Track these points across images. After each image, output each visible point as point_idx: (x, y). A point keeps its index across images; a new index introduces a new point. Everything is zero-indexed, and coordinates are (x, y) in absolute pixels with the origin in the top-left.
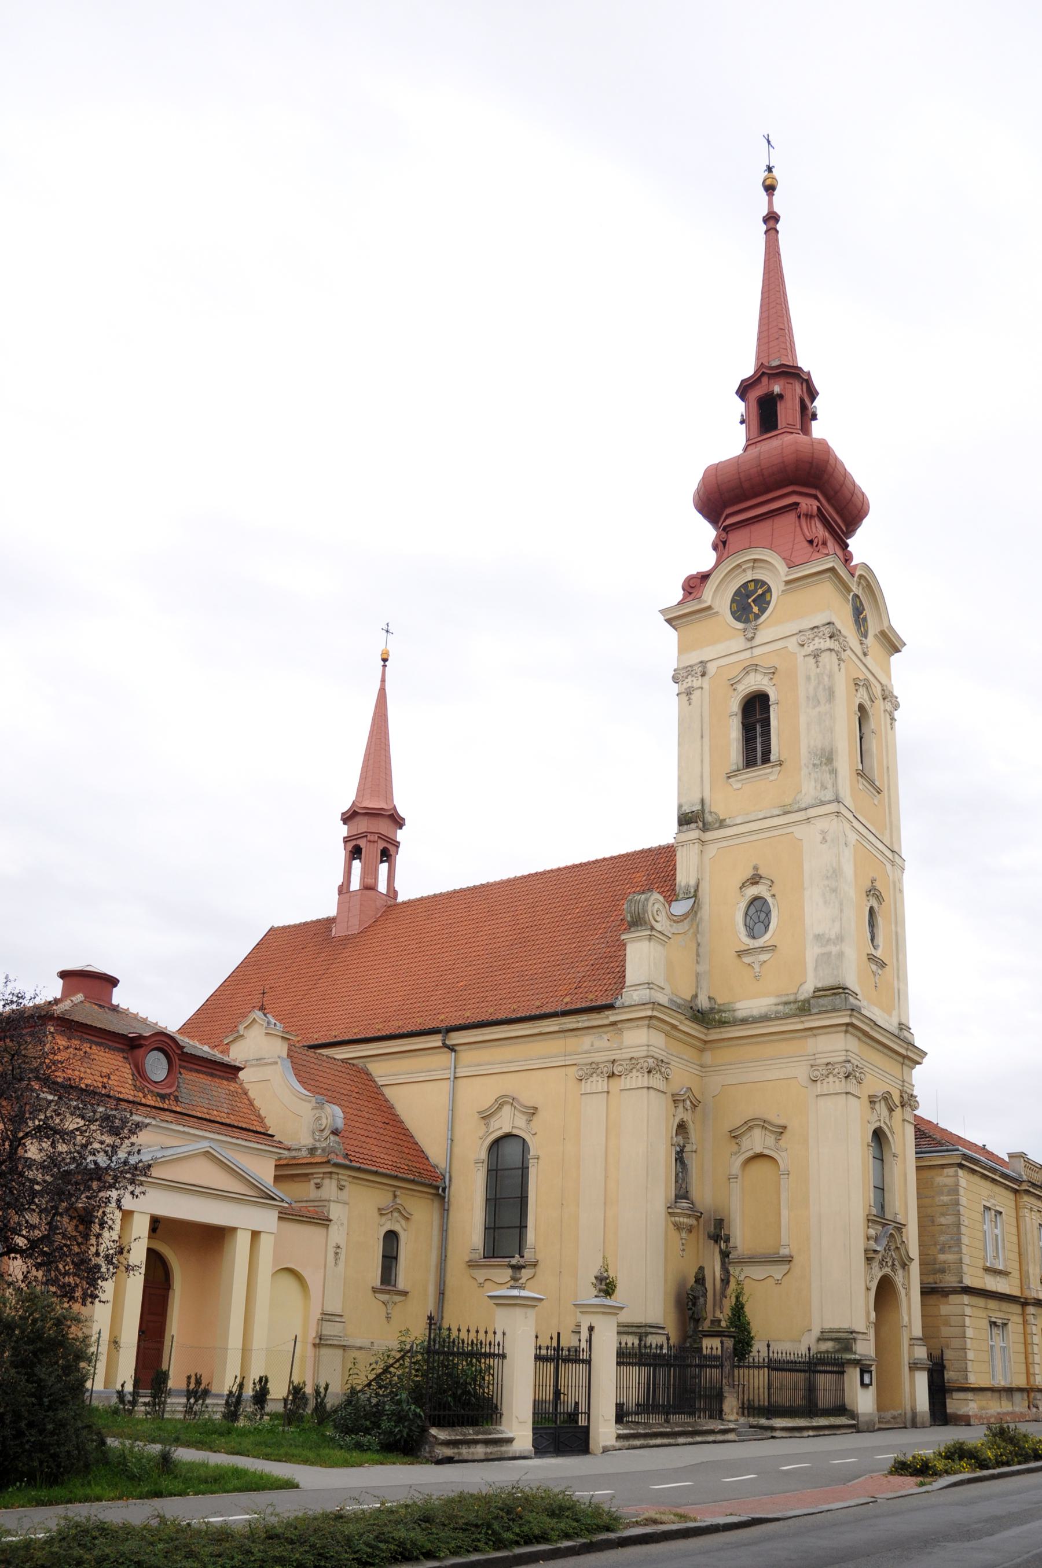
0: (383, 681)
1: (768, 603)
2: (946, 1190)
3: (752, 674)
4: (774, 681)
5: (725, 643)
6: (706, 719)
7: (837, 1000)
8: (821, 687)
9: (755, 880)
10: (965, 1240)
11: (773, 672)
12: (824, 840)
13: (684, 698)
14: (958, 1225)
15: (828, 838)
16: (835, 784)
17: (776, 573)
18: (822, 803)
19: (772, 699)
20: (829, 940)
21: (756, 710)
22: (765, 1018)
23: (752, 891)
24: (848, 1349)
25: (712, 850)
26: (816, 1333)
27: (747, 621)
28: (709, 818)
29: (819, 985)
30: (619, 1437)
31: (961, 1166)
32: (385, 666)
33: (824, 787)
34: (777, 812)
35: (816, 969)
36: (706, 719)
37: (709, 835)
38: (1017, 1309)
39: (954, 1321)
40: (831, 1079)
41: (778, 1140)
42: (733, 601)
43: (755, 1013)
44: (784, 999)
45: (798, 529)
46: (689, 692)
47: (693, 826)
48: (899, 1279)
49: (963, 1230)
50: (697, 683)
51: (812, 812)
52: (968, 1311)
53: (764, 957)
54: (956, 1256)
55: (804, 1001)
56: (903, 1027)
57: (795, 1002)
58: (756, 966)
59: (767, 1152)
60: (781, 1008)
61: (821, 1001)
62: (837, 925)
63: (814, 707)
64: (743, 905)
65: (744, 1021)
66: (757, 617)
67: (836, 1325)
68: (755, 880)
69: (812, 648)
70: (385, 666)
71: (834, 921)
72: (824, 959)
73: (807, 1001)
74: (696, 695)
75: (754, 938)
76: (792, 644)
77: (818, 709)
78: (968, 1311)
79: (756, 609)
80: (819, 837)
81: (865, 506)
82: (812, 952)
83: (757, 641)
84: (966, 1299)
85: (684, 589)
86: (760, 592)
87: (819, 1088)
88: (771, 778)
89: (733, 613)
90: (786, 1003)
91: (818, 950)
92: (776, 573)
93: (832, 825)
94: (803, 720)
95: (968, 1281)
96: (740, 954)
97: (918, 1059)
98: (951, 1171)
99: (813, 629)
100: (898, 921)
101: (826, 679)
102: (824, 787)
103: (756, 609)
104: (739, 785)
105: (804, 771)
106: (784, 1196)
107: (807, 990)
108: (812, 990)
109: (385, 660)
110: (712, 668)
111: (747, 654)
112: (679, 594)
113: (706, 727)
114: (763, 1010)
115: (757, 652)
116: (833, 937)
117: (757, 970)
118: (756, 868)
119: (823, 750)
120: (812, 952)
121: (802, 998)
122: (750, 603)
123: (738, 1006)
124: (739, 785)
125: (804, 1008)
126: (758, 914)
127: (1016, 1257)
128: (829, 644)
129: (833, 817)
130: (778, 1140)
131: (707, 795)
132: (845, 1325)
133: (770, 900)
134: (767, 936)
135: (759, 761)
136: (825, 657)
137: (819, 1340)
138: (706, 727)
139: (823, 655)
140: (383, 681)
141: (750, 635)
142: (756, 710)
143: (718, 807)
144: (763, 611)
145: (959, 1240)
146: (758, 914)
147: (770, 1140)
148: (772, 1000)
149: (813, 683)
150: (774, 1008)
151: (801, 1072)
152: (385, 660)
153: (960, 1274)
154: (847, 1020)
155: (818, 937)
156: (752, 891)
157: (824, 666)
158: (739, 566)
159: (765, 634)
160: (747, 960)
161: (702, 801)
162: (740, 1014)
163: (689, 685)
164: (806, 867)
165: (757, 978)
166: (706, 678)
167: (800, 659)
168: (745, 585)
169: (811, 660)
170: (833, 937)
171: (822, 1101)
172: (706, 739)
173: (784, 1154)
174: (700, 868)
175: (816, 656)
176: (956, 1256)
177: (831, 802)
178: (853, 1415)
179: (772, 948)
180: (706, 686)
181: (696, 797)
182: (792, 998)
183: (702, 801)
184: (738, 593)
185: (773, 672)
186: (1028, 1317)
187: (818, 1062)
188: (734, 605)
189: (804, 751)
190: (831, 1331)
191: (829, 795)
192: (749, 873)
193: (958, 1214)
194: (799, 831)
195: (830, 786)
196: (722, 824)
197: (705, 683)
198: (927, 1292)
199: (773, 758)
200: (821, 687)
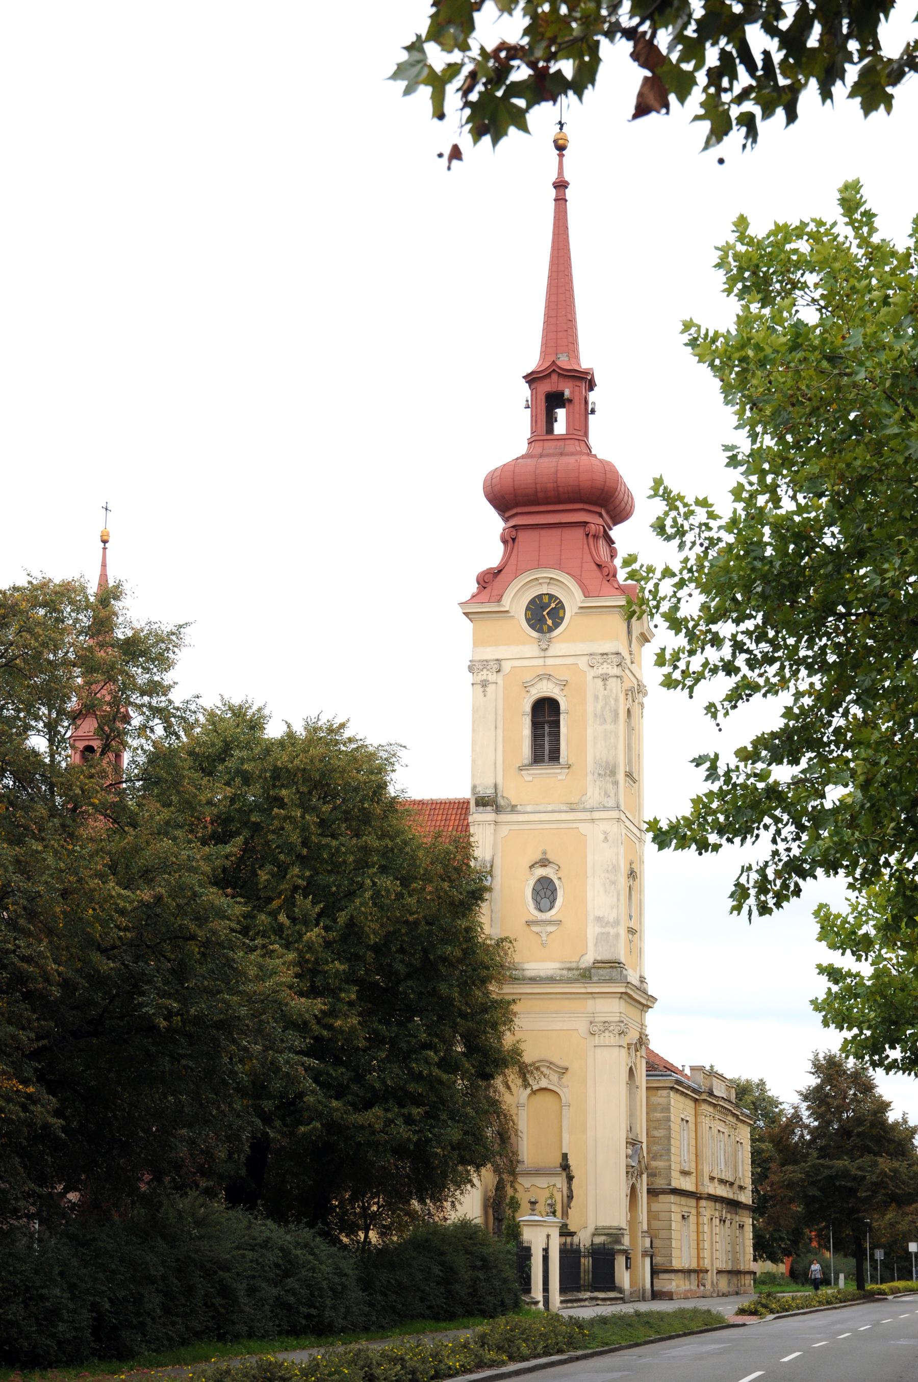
0: (104, 565)
1: (562, 619)
2: (659, 1108)
3: (545, 682)
4: (565, 693)
5: (520, 648)
6: (500, 712)
7: (614, 973)
8: (608, 708)
9: (544, 862)
10: (673, 1150)
11: (564, 684)
12: (606, 839)
13: (479, 689)
14: (669, 1138)
15: (610, 839)
16: (616, 794)
17: (571, 596)
18: (605, 808)
19: (563, 707)
20: (607, 923)
21: (546, 713)
22: (551, 980)
23: (540, 872)
24: (619, 1242)
25: (504, 831)
26: (591, 1229)
27: (540, 631)
28: (501, 802)
29: (599, 958)
30: (562, 1302)
31: (672, 1088)
32: (105, 549)
33: (607, 795)
34: (564, 807)
35: (596, 945)
36: (500, 712)
37: (502, 817)
38: (692, 1202)
39: (662, 1216)
40: (607, 1034)
41: (560, 1079)
42: (528, 609)
43: (542, 974)
44: (568, 965)
45: (586, 547)
46: (484, 684)
47: (489, 808)
48: (638, 1186)
49: (672, 1141)
50: (492, 677)
51: (596, 815)
52: (674, 1208)
53: (550, 929)
54: (667, 1164)
55: (585, 969)
56: (642, 980)
57: (577, 969)
58: (544, 936)
59: (550, 1087)
60: (565, 972)
61: (601, 972)
62: (615, 911)
63: (601, 725)
64: (532, 882)
65: (533, 980)
66: (550, 630)
67: (608, 1224)
68: (544, 862)
69: (600, 671)
70: (105, 549)
71: (612, 908)
72: (602, 938)
73: (588, 970)
74: (491, 689)
75: (540, 910)
76: (583, 662)
77: (604, 727)
78: (674, 1208)
79: (550, 622)
80: (602, 837)
81: (628, 507)
82: (593, 931)
83: (550, 653)
84: (672, 1198)
85: (478, 583)
86: (553, 605)
87: (597, 1040)
88: (560, 777)
89: (528, 620)
90: (569, 969)
91: (598, 930)
92: (571, 596)
93: (614, 829)
94: (589, 732)
95: (675, 1184)
96: (529, 923)
97: (649, 1004)
98: (664, 1093)
99: (603, 654)
100: (641, 892)
101: (613, 702)
102: (607, 795)
103: (550, 622)
104: (530, 778)
105: (590, 777)
106: (565, 1123)
107: (588, 960)
108: (592, 961)
109: (105, 542)
110: (507, 666)
111: (540, 662)
112: (474, 587)
113: (500, 718)
114: (550, 973)
115: (550, 662)
116: (611, 920)
117: (544, 938)
118: (544, 853)
119: (607, 763)
120: (593, 931)
121: (583, 966)
122: (544, 615)
123: (526, 966)
124: (530, 778)
125: (586, 975)
126: (545, 892)
127: (693, 1157)
128: (616, 671)
129: (614, 822)
130: (560, 1079)
131: (500, 782)
132: (615, 1224)
133: (556, 882)
134: (553, 912)
135: (546, 758)
136: (612, 682)
137: (594, 1235)
138: (500, 718)
139: (611, 680)
140: (104, 565)
141: (545, 647)
142: (546, 713)
143: (511, 792)
144: (557, 625)
145: (669, 1150)
146: (545, 892)
147: (554, 1077)
148: (557, 965)
149: (601, 703)
150: (559, 972)
151: (582, 1026)
152: (105, 542)
153: (669, 1178)
154: (623, 990)
155: (598, 919)
156: (540, 872)
157: (611, 690)
158: (536, 579)
159: (557, 648)
160: (535, 929)
161: (496, 786)
162: (529, 974)
163: (484, 677)
164: (590, 859)
165: (543, 945)
166: (500, 674)
167: (589, 678)
168: (540, 597)
169: (599, 682)
170: (611, 920)
171: (599, 1051)
172: (500, 731)
173: (565, 1090)
174: (494, 846)
175: (605, 678)
176: (667, 1164)
177: (612, 809)
178: (621, 1291)
179: (558, 923)
180: (500, 682)
181: (490, 782)
182: (574, 965)
183: (496, 786)
184: (532, 602)
185: (564, 684)
186: (701, 1210)
187: (597, 1019)
188: (529, 613)
189: (590, 759)
190: (604, 1228)
191: (611, 803)
192: (538, 856)
193: (669, 1128)
194: (584, 828)
195: (612, 795)
196: (513, 809)
197: (500, 678)
198: (649, 1191)
199: (562, 760)
200: (608, 708)
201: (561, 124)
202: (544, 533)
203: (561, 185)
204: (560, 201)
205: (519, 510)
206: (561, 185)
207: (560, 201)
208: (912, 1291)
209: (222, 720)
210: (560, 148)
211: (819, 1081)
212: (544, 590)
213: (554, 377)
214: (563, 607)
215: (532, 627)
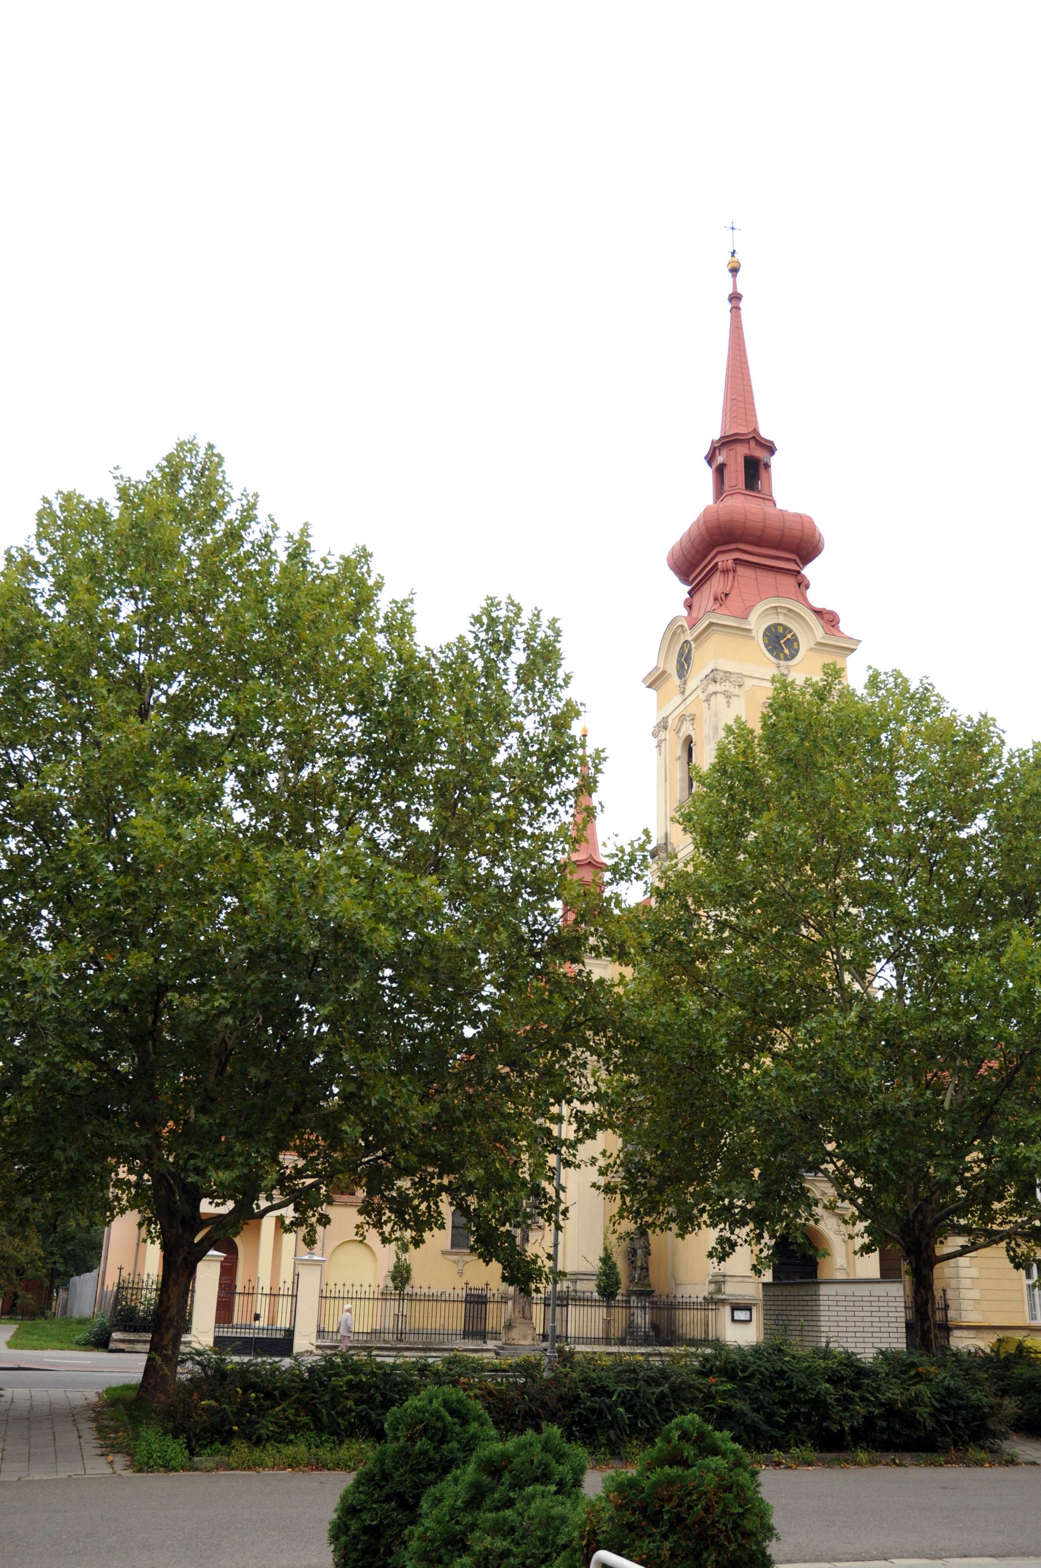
27: (777, 657)
50: (736, 691)
74: (733, 700)
79: (786, 651)
89: (766, 645)
110: (749, 683)
144: (793, 656)
201: (733, 253)
202: (760, 572)
203: (735, 298)
204: (736, 310)
205: (734, 546)
206: (735, 298)
207: (736, 310)
208: (939, 1411)
209: (425, 665)
210: (734, 271)
211: (142, 1360)
212: (781, 620)
213: (753, 443)
214: (796, 640)
215: (770, 651)
